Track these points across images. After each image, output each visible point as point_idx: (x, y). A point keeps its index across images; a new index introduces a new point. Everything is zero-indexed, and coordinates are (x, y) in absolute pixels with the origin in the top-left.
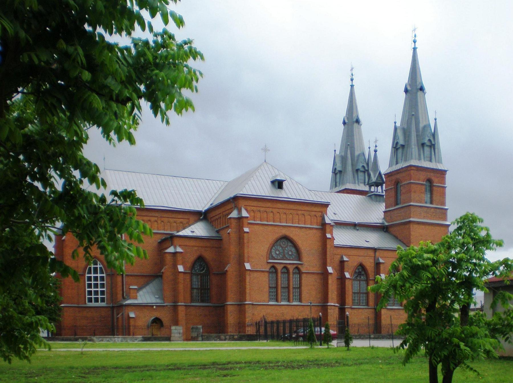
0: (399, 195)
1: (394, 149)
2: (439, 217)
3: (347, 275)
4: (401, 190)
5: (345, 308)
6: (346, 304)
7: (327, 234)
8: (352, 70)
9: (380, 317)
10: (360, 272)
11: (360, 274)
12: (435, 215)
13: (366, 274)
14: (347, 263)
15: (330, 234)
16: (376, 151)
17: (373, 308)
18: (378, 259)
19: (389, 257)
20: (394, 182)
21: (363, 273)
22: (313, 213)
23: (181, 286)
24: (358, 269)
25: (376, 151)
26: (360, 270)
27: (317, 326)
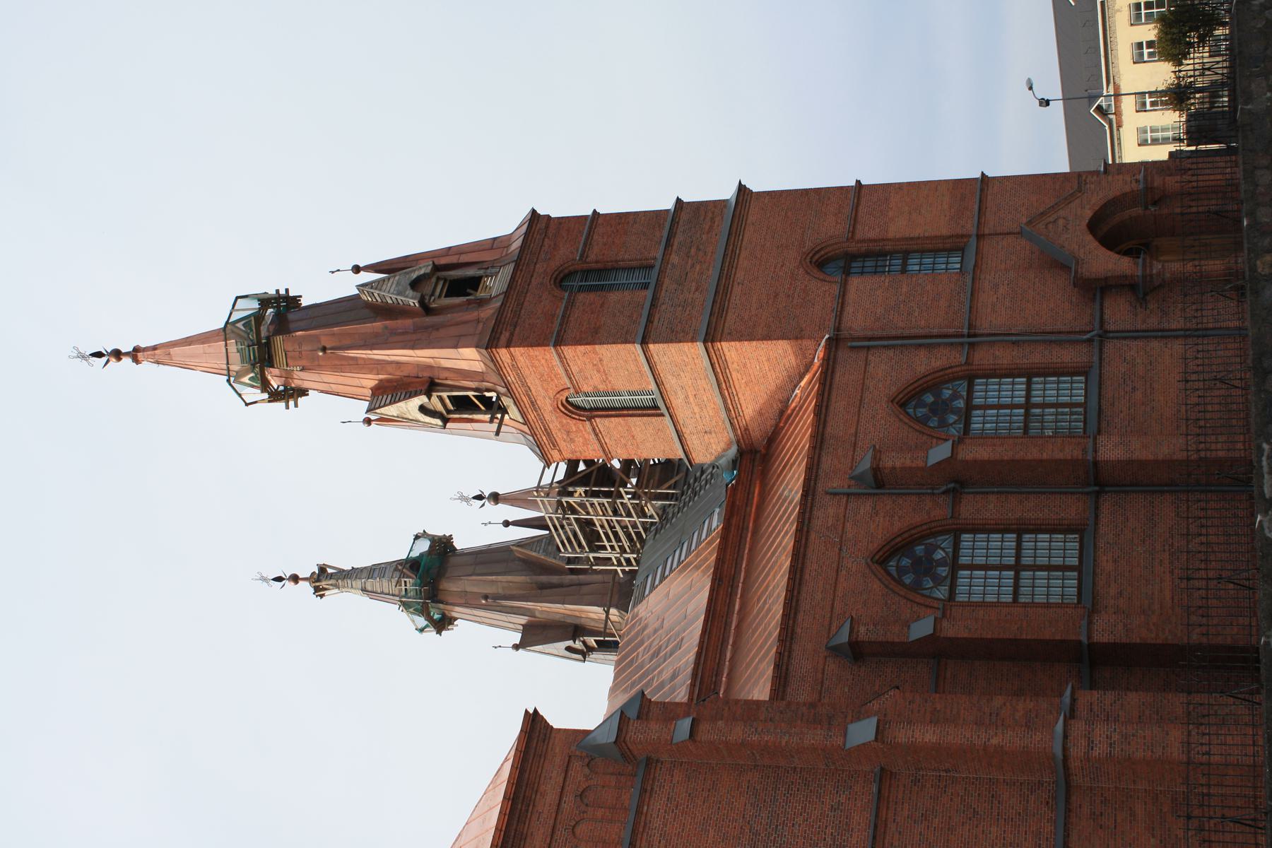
0: (615, 400)
1: (449, 425)
2: (708, 232)
3: (922, 628)
4: (597, 393)
5: (1089, 645)
6: (1073, 637)
7: (910, 640)
8: (264, 579)
9: (1142, 464)
10: (917, 562)
11: (925, 567)
12: (698, 249)
13: (920, 539)
14: (862, 629)
15: (679, 722)
16: (495, 498)
17: (1097, 502)
18: (859, 479)
19: (853, 431)
20: (572, 422)
21: (919, 549)
22: (569, 803)
23: (1202, 496)
24: (902, 571)
25: (495, 498)
26: (906, 562)
27: (1210, 49)
